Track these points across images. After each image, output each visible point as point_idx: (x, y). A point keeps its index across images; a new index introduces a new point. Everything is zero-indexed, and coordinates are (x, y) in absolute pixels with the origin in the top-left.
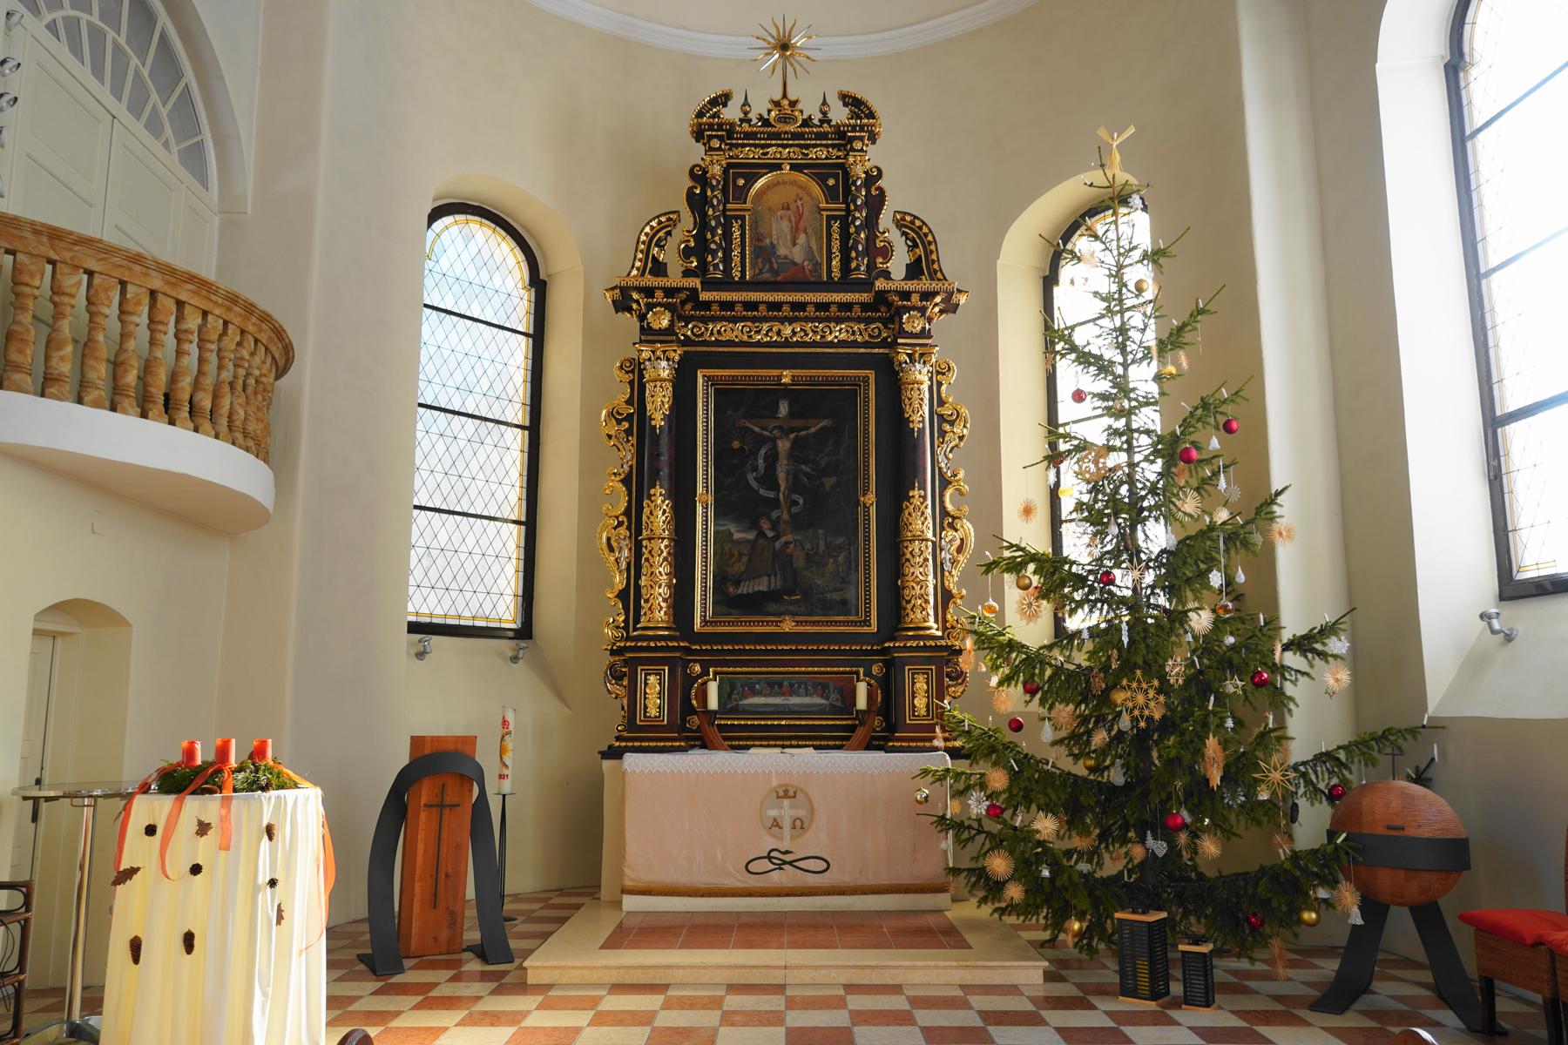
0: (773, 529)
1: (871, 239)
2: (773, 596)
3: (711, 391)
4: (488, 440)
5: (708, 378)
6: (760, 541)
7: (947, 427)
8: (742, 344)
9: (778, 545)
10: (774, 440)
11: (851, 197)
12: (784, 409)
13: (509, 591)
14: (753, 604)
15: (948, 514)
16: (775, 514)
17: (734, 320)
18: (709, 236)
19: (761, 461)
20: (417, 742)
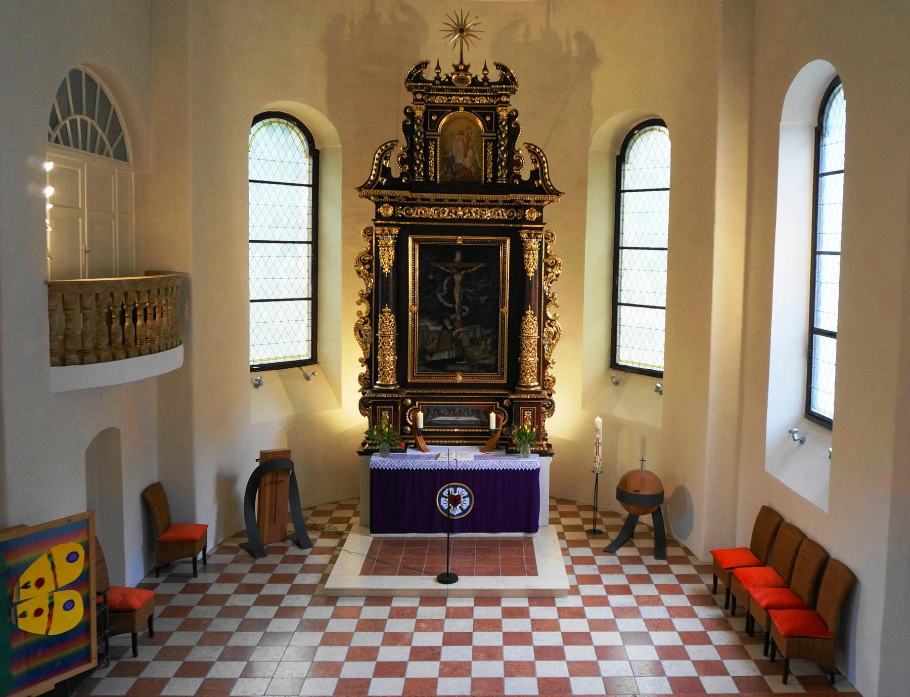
1: (510, 157)
2: (451, 361)
3: (417, 246)
4: (289, 254)
5: (414, 241)
6: (445, 331)
7: (550, 270)
8: (434, 220)
9: (454, 333)
10: (452, 275)
11: (502, 132)
12: (458, 257)
13: (306, 318)
14: (440, 366)
15: (548, 318)
16: (452, 317)
17: (430, 206)
18: (415, 154)
19: (445, 287)
20: (262, 453)
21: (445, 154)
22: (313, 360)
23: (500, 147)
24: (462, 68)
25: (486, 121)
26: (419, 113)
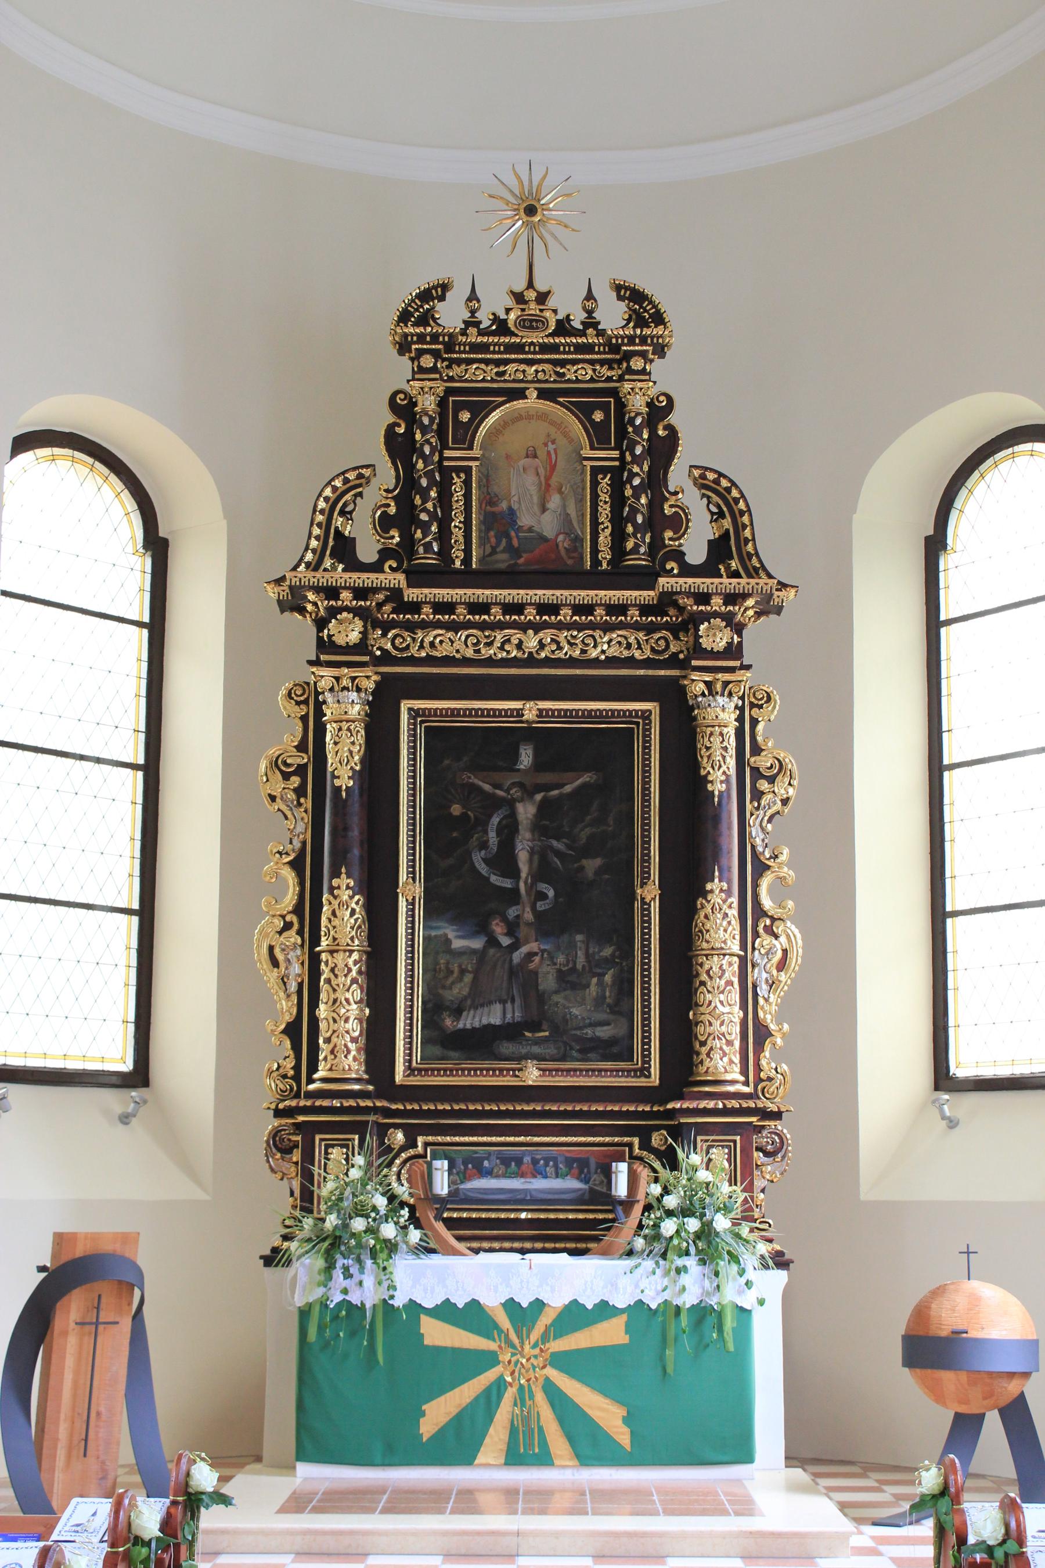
0: (510, 933)
2: (511, 1032)
3: (420, 731)
6: (492, 951)
8: (466, 662)
9: (517, 957)
10: (511, 803)
11: (635, 443)
12: (526, 757)
14: (479, 1044)
15: (765, 914)
16: (512, 912)
18: (418, 501)
22: (139, 1076)
23: (630, 480)
24: (531, 297)
25: (592, 422)
26: (428, 403)
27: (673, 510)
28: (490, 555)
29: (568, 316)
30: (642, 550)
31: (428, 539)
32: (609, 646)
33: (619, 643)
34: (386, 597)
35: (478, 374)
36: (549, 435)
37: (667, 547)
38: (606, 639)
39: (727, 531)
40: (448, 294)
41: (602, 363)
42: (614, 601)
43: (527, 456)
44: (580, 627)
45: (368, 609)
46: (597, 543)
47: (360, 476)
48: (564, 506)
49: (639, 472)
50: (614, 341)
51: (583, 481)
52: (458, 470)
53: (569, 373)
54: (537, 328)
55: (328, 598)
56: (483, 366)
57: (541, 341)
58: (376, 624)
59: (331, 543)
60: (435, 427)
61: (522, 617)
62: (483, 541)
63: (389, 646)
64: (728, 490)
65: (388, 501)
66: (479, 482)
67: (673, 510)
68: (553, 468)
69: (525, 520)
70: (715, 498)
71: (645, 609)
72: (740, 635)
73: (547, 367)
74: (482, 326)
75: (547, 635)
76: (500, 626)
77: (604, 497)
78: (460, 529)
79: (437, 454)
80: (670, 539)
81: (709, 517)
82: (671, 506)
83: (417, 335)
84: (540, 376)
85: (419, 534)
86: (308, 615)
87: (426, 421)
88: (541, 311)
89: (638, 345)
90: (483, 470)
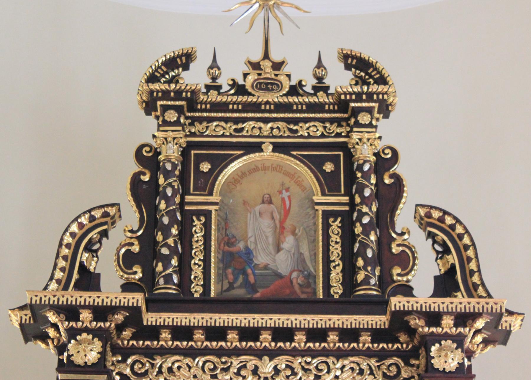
1: (384, 242)
11: (361, 190)
18: (160, 237)
21: (229, 244)
23: (359, 219)
27: (401, 249)
28: (228, 290)
29: (300, 82)
30: (373, 281)
31: (168, 272)
32: (342, 372)
33: (352, 369)
34: (126, 318)
35: (218, 131)
36: (283, 184)
37: (394, 282)
38: (339, 365)
39: (453, 266)
40: (192, 65)
41: (332, 121)
42: (347, 325)
43: (263, 202)
44: (314, 354)
45: (107, 330)
46: (329, 279)
47: (106, 215)
48: (298, 247)
49: (368, 212)
50: (343, 97)
51: (315, 224)
52: (198, 214)
53: (303, 130)
54: (273, 90)
55: (68, 319)
56: (223, 124)
57: (276, 100)
58: (116, 350)
59: (75, 276)
60: (177, 172)
61: (258, 344)
62: (221, 277)
63: (128, 371)
64: (453, 227)
65: (132, 241)
66: (218, 225)
67: (401, 249)
68: (287, 212)
69: (261, 258)
70: (441, 236)
71: (378, 335)
72: (469, 360)
73: (281, 124)
74: (222, 91)
75: (281, 362)
76: (237, 352)
77: (335, 238)
78: (199, 266)
79: (178, 196)
80: (399, 275)
81: (434, 255)
82: (399, 245)
83: (163, 91)
84: (275, 132)
85: (160, 267)
86: (50, 342)
87: (169, 167)
88: (276, 75)
89: (365, 101)
90: (222, 214)
